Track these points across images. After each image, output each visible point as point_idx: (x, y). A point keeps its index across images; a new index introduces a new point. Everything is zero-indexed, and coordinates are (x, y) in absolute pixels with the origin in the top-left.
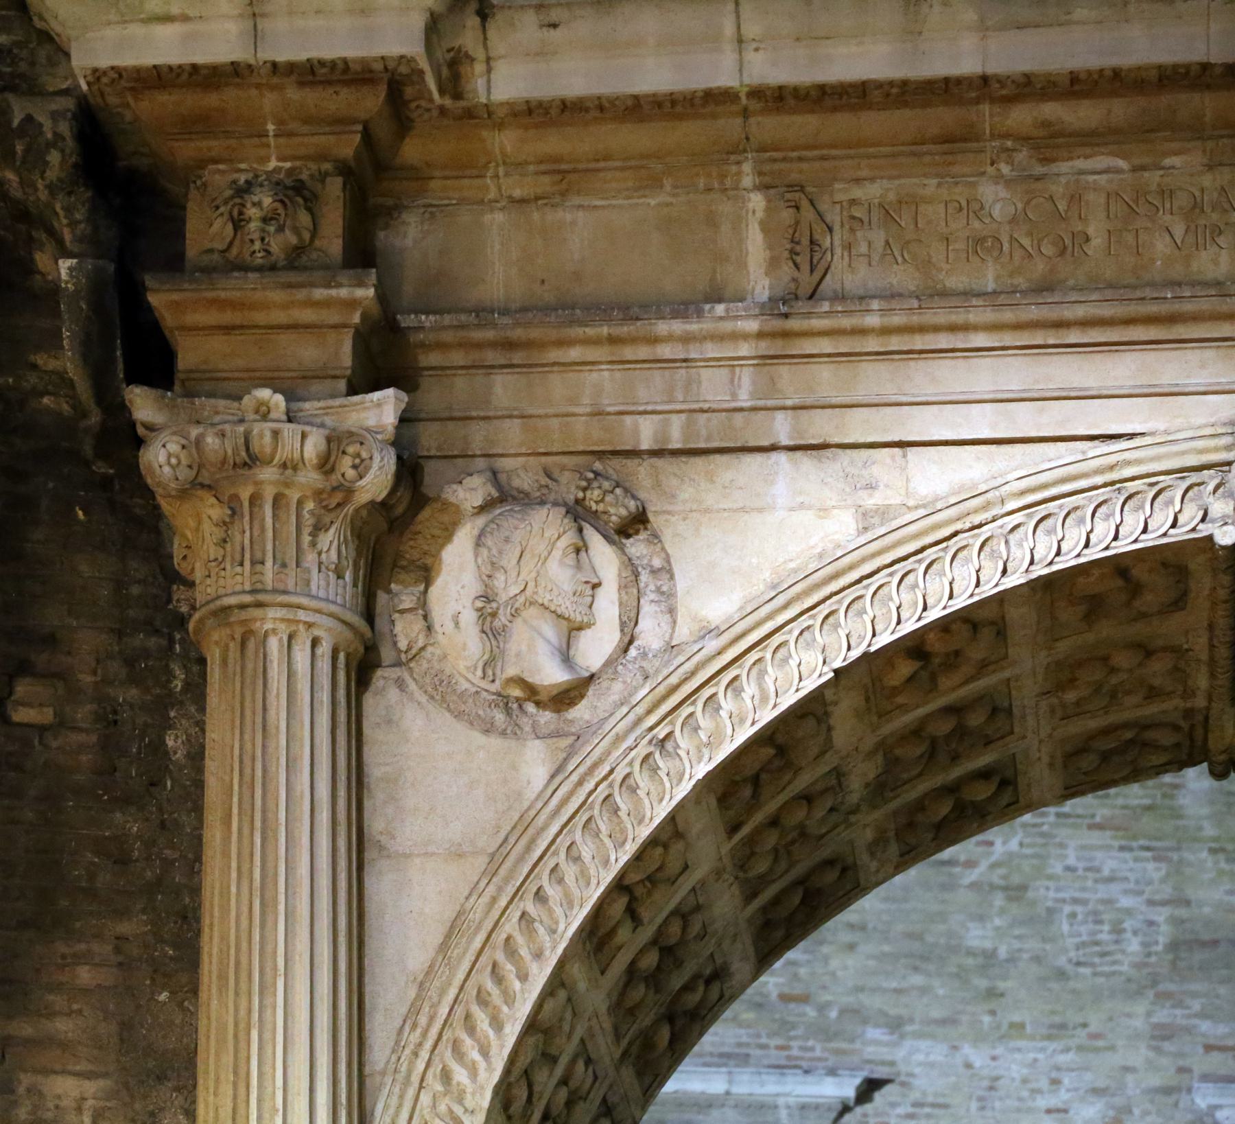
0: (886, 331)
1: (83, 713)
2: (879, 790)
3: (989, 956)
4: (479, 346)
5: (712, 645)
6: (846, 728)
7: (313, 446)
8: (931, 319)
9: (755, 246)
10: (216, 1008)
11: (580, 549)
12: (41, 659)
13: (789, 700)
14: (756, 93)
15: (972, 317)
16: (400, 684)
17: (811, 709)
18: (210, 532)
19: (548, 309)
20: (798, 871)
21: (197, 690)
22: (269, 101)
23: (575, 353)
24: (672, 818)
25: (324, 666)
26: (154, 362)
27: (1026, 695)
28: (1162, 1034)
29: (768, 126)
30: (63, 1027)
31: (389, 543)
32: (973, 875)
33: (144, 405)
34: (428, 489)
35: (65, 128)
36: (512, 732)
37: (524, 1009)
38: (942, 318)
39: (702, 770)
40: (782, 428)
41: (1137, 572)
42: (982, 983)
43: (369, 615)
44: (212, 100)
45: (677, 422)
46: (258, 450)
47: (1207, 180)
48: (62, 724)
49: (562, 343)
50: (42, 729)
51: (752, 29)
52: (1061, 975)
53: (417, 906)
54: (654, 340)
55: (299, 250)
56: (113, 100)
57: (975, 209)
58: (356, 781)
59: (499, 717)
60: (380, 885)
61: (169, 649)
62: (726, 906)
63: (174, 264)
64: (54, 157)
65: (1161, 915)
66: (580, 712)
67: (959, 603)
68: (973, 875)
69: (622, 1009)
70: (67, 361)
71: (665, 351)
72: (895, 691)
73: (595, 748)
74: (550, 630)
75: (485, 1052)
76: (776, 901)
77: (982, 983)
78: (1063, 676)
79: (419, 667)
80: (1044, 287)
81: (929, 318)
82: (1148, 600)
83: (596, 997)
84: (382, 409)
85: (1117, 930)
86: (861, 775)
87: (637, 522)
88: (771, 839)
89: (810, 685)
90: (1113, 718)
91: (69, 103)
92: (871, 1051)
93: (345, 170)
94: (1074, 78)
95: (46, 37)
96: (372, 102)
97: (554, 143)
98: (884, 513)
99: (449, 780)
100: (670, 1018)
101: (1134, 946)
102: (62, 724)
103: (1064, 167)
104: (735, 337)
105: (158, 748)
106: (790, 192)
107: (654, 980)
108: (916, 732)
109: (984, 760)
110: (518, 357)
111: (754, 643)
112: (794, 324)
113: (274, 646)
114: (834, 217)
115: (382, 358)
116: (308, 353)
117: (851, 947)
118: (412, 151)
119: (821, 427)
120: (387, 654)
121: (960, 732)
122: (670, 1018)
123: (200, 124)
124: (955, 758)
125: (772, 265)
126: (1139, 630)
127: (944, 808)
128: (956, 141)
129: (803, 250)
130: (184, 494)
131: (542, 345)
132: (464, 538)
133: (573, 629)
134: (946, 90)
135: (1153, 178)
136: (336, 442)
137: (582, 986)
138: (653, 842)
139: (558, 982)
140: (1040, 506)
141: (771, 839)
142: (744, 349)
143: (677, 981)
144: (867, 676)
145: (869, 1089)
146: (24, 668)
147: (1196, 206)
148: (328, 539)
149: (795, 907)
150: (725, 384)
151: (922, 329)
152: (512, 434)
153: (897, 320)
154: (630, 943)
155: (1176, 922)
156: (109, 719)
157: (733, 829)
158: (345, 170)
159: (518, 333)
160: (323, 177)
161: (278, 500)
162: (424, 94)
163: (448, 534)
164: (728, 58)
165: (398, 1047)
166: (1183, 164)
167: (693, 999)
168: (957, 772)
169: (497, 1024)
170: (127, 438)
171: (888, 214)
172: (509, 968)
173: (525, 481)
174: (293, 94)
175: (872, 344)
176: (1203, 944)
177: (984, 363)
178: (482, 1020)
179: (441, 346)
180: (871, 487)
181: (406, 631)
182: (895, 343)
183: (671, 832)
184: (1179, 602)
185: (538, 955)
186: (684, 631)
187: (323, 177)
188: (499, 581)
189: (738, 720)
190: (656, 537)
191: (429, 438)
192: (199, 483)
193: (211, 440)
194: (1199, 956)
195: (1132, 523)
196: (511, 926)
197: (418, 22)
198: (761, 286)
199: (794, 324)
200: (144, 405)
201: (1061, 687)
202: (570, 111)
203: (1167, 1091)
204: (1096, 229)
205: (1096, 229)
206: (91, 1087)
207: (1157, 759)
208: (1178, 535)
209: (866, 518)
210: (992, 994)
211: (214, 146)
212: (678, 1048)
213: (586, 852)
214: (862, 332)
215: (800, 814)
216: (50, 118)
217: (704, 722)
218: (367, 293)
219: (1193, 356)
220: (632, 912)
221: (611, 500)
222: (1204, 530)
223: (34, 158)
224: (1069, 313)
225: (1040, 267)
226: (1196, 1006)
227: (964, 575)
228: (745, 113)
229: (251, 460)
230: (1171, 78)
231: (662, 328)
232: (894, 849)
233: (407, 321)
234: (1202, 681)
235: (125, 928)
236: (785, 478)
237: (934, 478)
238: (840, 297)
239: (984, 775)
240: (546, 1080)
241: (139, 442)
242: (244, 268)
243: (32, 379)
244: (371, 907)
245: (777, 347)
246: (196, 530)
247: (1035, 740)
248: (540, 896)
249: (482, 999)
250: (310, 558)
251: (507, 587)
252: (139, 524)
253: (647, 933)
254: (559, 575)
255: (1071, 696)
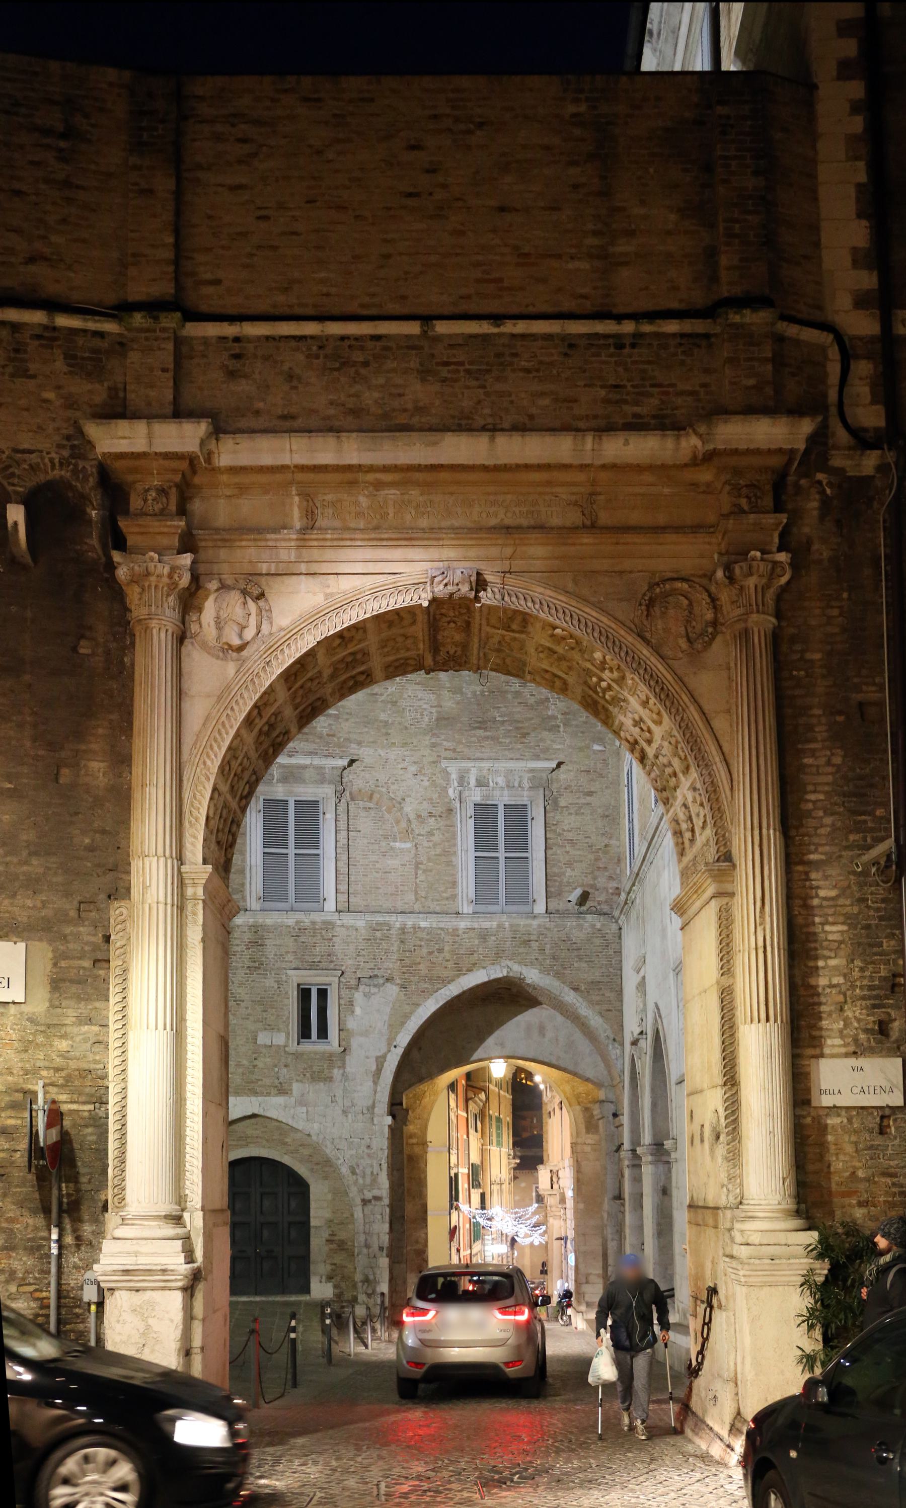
0: (332, 540)
1: (100, 650)
2: (333, 677)
3: (386, 722)
4: (216, 540)
5: (282, 633)
6: (321, 657)
7: (166, 570)
8: (345, 535)
9: (296, 513)
10: (137, 743)
11: (245, 603)
12: (88, 634)
13: (304, 650)
14: (296, 466)
15: (356, 536)
16: (192, 644)
17: (311, 653)
18: (136, 596)
19: (236, 529)
20: (310, 701)
21: (133, 644)
22: (155, 464)
23: (244, 543)
24: (271, 685)
25: (170, 637)
26: (120, 543)
27: (373, 649)
28: (433, 745)
29: (299, 476)
30: (94, 746)
31: (189, 601)
32: (383, 698)
33: (117, 556)
34: (201, 583)
35: (94, 470)
36: (225, 659)
37: (227, 743)
38: (348, 536)
39: (279, 671)
40: (303, 568)
41: (402, 614)
42: (384, 731)
43: (183, 623)
44: (137, 463)
45: (273, 565)
46: (151, 570)
47: (421, 499)
48: (94, 654)
49: (241, 540)
50: (88, 655)
51: (294, 447)
52: (406, 728)
53: (197, 711)
54: (267, 540)
55: (163, 509)
56: (109, 462)
57: (357, 504)
58: (179, 674)
59: (221, 654)
60: (186, 705)
61: (123, 631)
62: (289, 712)
63: (126, 512)
64: (91, 479)
65: (434, 710)
66: (244, 653)
67: (353, 622)
68: (383, 698)
69: (258, 743)
70: (95, 542)
71: (270, 543)
72: (335, 648)
73: (249, 664)
74: (236, 628)
75: (216, 756)
76: (304, 710)
77: (384, 731)
78: (383, 644)
79: (198, 638)
80: (377, 528)
81: (345, 536)
82: (406, 622)
83: (249, 738)
84: (186, 559)
85: (422, 715)
86: (327, 673)
87: (262, 595)
88: (301, 692)
89: (310, 646)
90: (399, 656)
91: (95, 463)
92: (352, 751)
93: (177, 486)
94: (384, 466)
95: (89, 442)
96: (185, 465)
97: (237, 479)
98: (332, 594)
99: (206, 672)
100: (273, 745)
101: (426, 719)
102: (94, 654)
103: (382, 492)
104: (290, 540)
105: (122, 662)
106: (307, 497)
107: (267, 734)
108: (342, 660)
109: (362, 668)
110: (228, 544)
111: (295, 633)
112: (307, 537)
113: (155, 631)
114: (318, 505)
115: (188, 544)
116: (165, 541)
117: (347, 720)
118: (197, 480)
119: (315, 568)
120: (188, 634)
121: (355, 660)
122: (273, 745)
123: (135, 470)
124: (354, 668)
125: (301, 518)
126: (402, 631)
127: (351, 683)
128: (353, 483)
129: (310, 514)
130: (128, 584)
131: (235, 541)
132: (211, 599)
133: (243, 628)
134: (349, 468)
135: (406, 497)
136: (173, 569)
137: (245, 736)
138: (265, 693)
139: (237, 735)
140: (375, 593)
141: (301, 692)
142: (293, 544)
143: (275, 734)
144: (328, 644)
145: (352, 762)
146: (82, 637)
147: (418, 506)
148: (171, 599)
149: (310, 710)
150: (287, 554)
151: (342, 539)
152: (225, 568)
153: (335, 536)
154: (259, 723)
155: (438, 712)
156: (108, 653)
157: (289, 689)
158: (177, 486)
159: (228, 537)
160: (170, 487)
161: (156, 587)
162: (200, 463)
163: (207, 597)
164: (288, 455)
165: (191, 754)
166: (414, 493)
167: (279, 739)
168: (354, 672)
169: (219, 747)
170: (111, 567)
171: (333, 504)
172: (223, 731)
173: (229, 581)
174: (161, 462)
175: (329, 543)
176: (445, 719)
177: (360, 550)
178: (216, 748)
179: (205, 540)
180: (328, 586)
181: (194, 628)
182: (335, 543)
183: (271, 690)
184: (414, 623)
185: (231, 727)
186: (274, 630)
187: (170, 487)
188: (221, 612)
189: (290, 656)
190: (267, 600)
191: (202, 568)
192: (134, 581)
193: (136, 568)
194: (444, 722)
195: (400, 599)
196: (224, 718)
197: (198, 441)
198: (298, 525)
199: (307, 537)
200: (117, 556)
201: (383, 647)
202: (243, 470)
203: (434, 762)
204: (391, 511)
205: (391, 511)
206: (102, 765)
207: (410, 669)
208: (412, 603)
209: (327, 596)
210: (387, 734)
211: (139, 476)
212: (276, 754)
213: (246, 696)
214: (326, 540)
215: (309, 684)
216: (91, 468)
217: (280, 657)
218: (183, 523)
219: (417, 550)
220: (260, 714)
221: (254, 589)
222: (420, 602)
223: (86, 479)
224: (383, 536)
225: (375, 522)
226: (443, 737)
227: (354, 613)
228: (293, 472)
229: (148, 574)
230: (410, 468)
231: (269, 536)
232: (337, 695)
233: (195, 532)
234: (421, 646)
235: (112, 717)
236: (304, 583)
237: (346, 584)
238: (320, 529)
239: (362, 673)
240: (235, 764)
241: (115, 568)
242: (146, 515)
243: (85, 547)
244: (183, 712)
245: (302, 543)
246: (133, 594)
247: (376, 663)
248: (232, 709)
249: (216, 741)
250: (166, 605)
251: (223, 615)
252: (117, 594)
253: (265, 720)
254: (239, 611)
255: (386, 650)
